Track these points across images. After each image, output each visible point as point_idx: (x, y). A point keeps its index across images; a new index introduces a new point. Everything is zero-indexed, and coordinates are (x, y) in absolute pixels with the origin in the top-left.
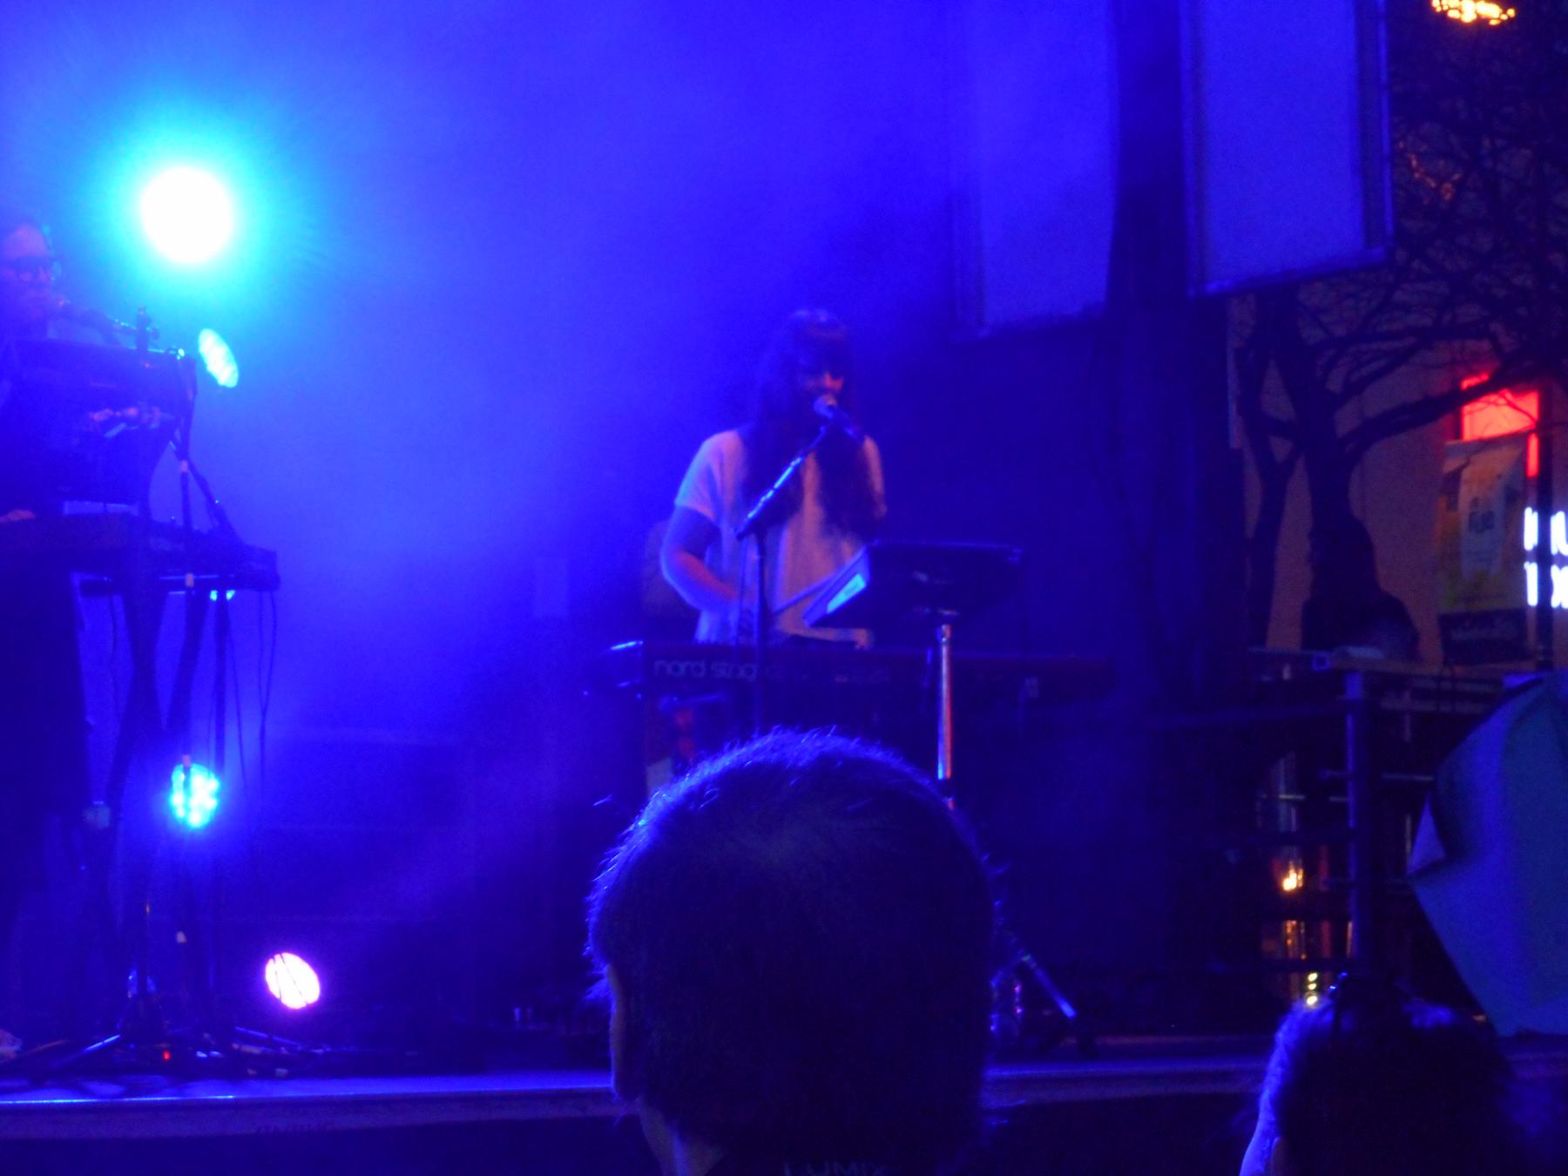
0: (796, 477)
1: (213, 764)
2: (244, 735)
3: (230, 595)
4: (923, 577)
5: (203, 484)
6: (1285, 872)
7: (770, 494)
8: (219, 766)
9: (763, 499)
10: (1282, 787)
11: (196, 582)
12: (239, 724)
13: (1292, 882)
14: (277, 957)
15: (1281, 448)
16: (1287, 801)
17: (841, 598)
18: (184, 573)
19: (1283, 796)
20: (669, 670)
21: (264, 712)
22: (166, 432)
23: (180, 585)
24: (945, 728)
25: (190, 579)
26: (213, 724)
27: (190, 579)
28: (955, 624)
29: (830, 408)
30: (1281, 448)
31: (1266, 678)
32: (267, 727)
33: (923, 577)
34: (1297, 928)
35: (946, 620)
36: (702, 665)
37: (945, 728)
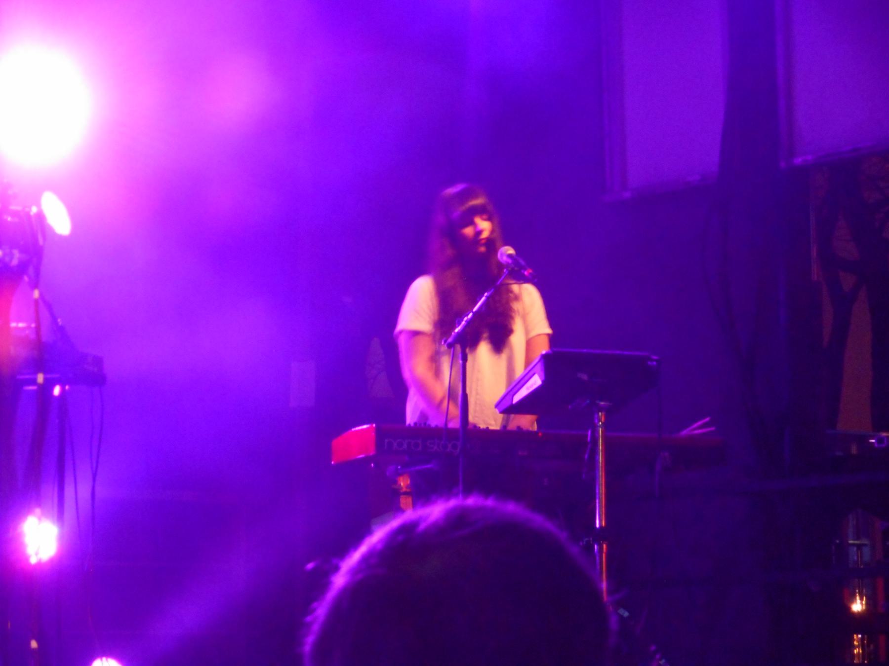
0: (437, 373)
1: (56, 517)
2: (80, 490)
3: (67, 387)
4: (585, 377)
5: (49, 307)
6: (852, 599)
7: (470, 315)
8: (60, 517)
9: (465, 319)
10: (851, 531)
11: (45, 379)
12: (74, 470)
13: (857, 606)
14: (104, 659)
15: (848, 281)
16: (853, 545)
17: (517, 398)
18: (36, 373)
19: (851, 542)
20: (395, 444)
21: (94, 480)
22: (22, 268)
23: (34, 382)
24: (601, 490)
25: (40, 378)
26: (56, 489)
27: (40, 378)
28: (608, 412)
29: (510, 256)
30: (848, 281)
31: (839, 454)
32: (98, 489)
33: (585, 377)
34: (862, 639)
35: (601, 409)
36: (420, 442)
37: (601, 490)
